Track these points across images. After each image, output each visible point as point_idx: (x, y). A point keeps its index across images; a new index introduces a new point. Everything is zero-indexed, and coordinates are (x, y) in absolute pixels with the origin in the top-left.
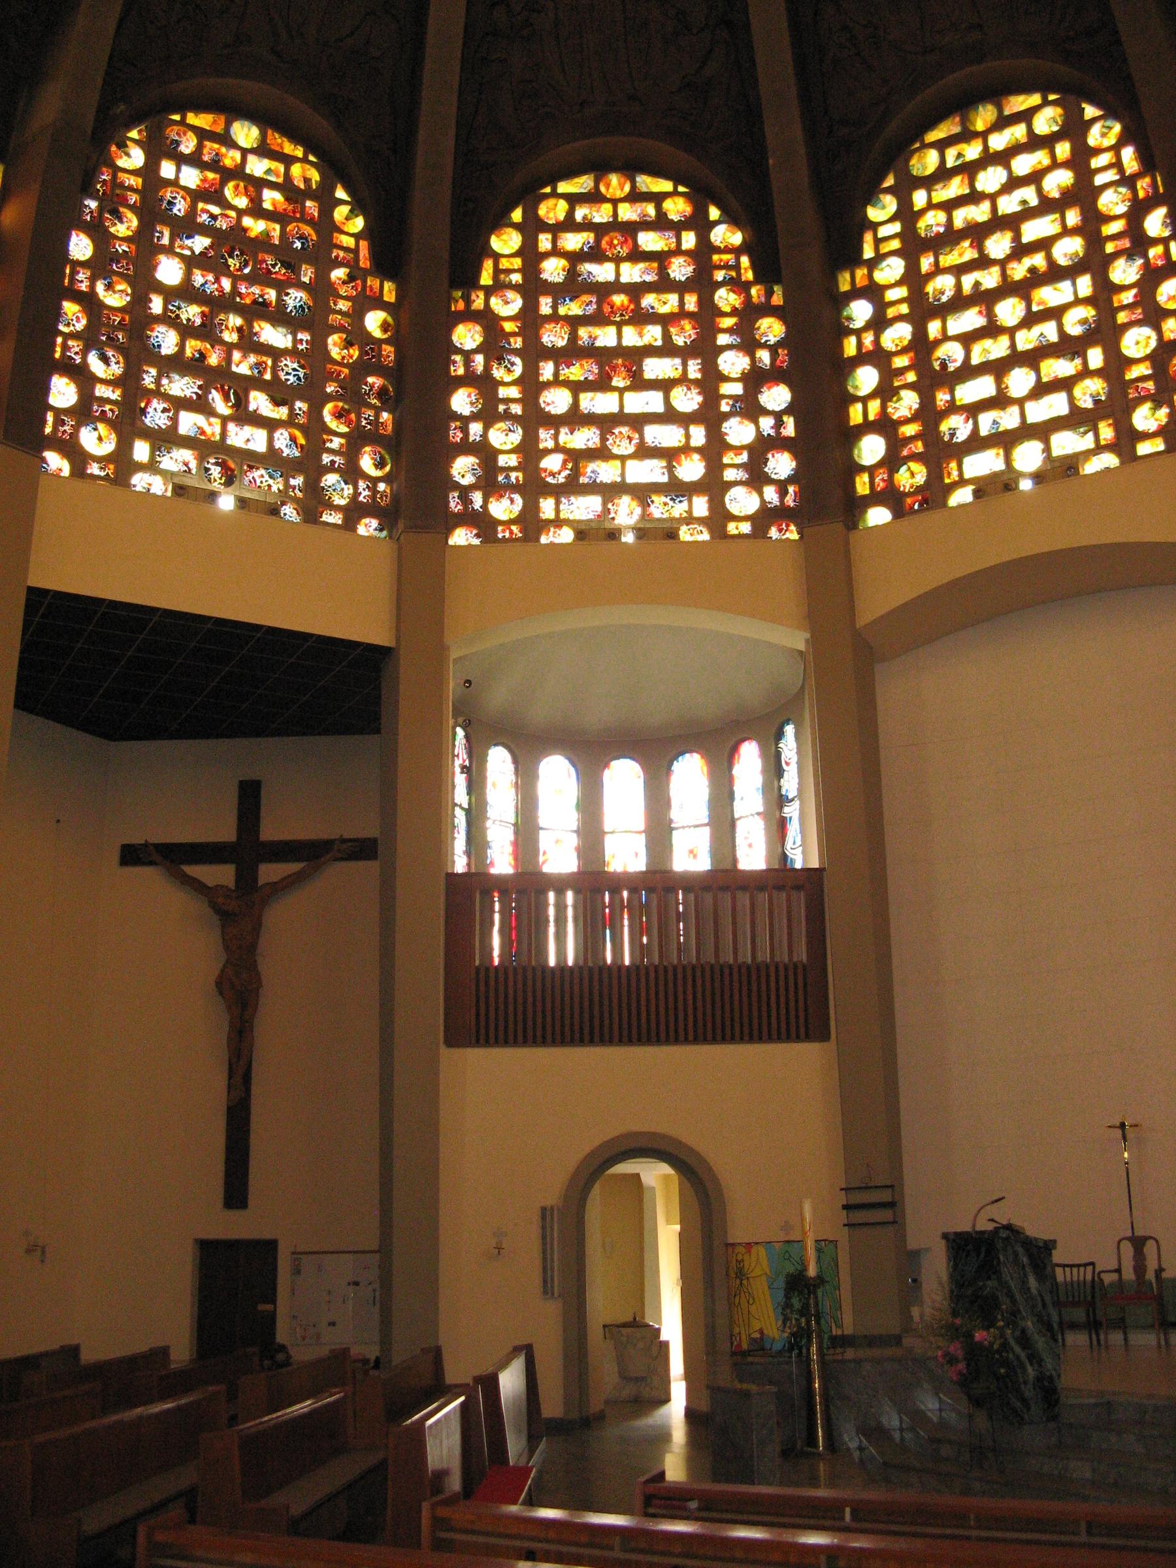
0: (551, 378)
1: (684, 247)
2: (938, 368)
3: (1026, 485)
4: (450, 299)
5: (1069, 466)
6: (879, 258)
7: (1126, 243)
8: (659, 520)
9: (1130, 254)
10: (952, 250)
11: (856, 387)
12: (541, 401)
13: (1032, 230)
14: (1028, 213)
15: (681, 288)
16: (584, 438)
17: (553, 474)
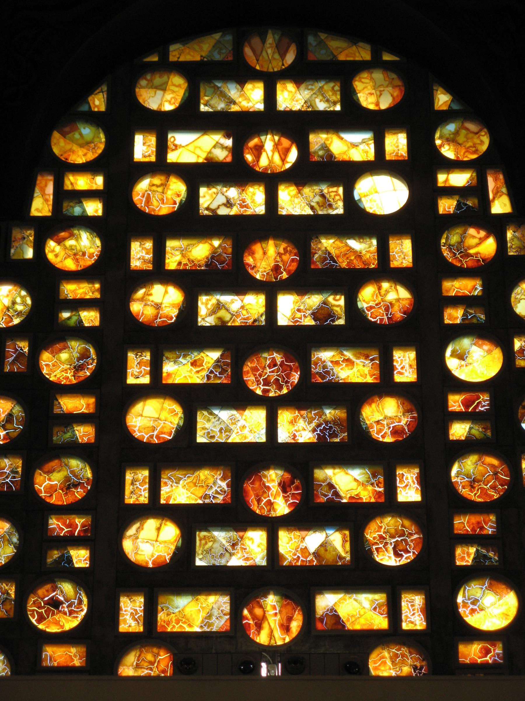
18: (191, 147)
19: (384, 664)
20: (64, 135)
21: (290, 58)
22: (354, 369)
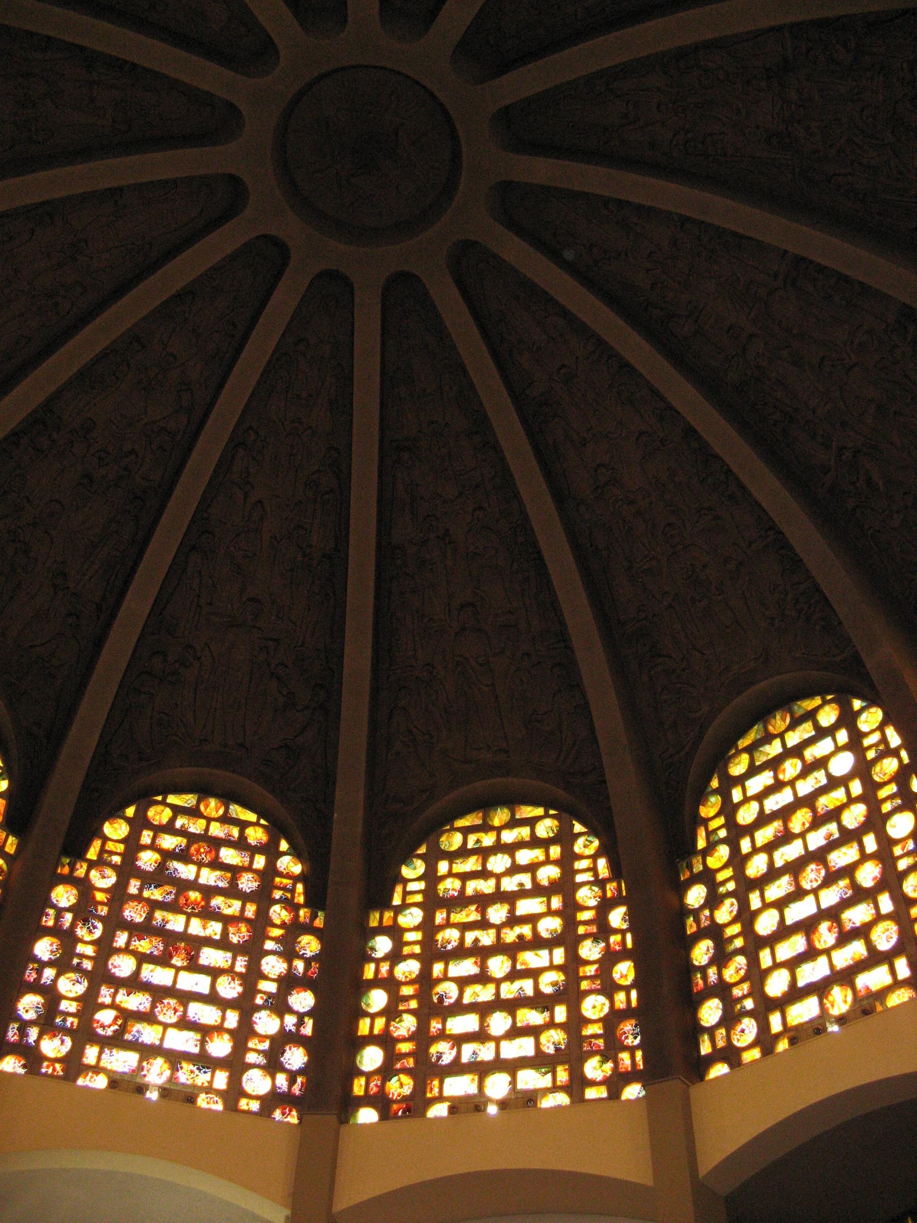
0: (123, 946)
1: (255, 867)
2: (436, 1001)
3: (492, 1110)
4: (58, 863)
5: (530, 1098)
6: (405, 906)
7: (593, 929)
8: (183, 1084)
9: (596, 938)
10: (461, 911)
11: (368, 1005)
12: (110, 963)
13: (525, 907)
14: (522, 893)
15: (245, 897)
16: (137, 1001)
17: (103, 1027)
20: (704, 805)
21: (788, 720)
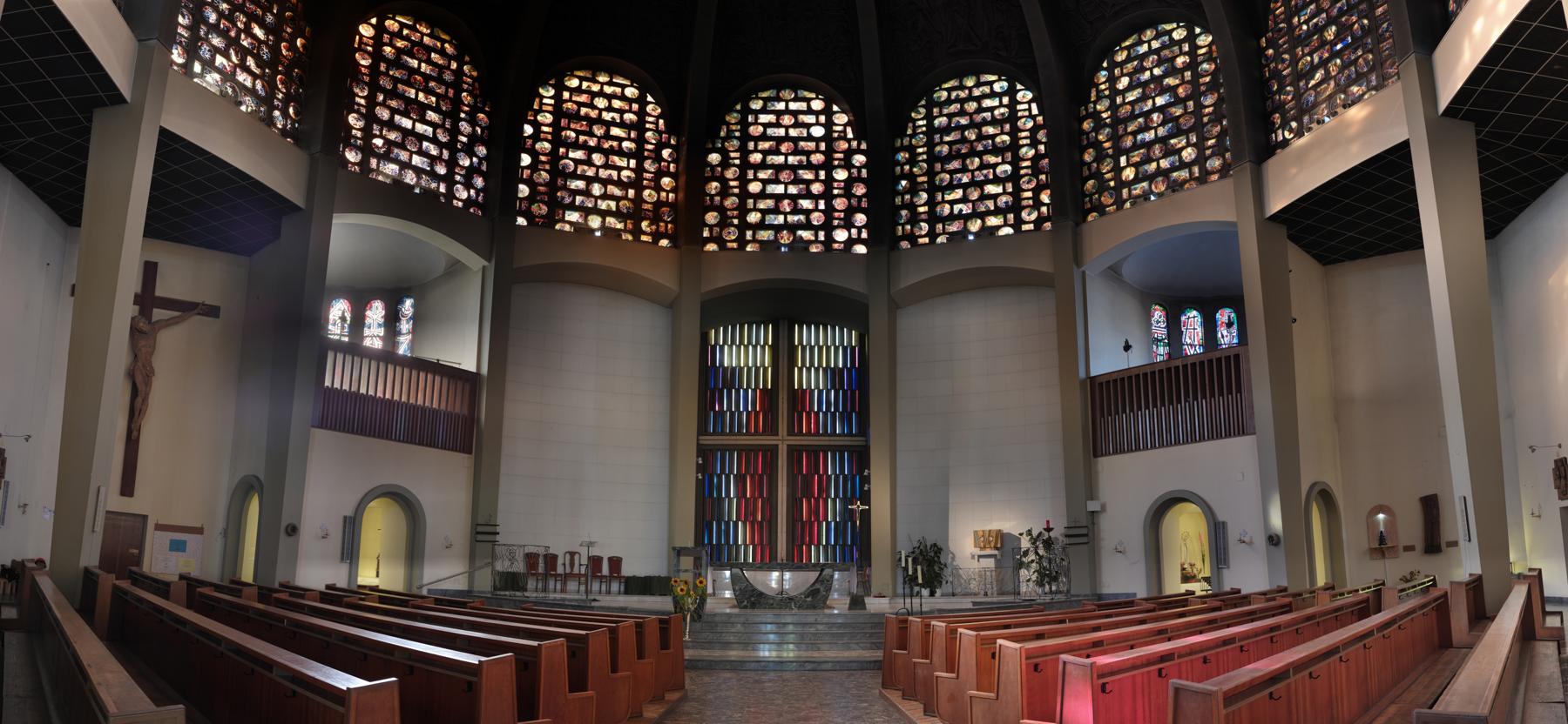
3: (971, 237)
18: (764, 118)
19: (814, 249)
22: (808, 175)
